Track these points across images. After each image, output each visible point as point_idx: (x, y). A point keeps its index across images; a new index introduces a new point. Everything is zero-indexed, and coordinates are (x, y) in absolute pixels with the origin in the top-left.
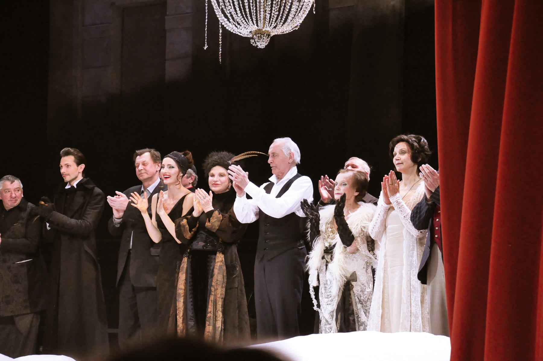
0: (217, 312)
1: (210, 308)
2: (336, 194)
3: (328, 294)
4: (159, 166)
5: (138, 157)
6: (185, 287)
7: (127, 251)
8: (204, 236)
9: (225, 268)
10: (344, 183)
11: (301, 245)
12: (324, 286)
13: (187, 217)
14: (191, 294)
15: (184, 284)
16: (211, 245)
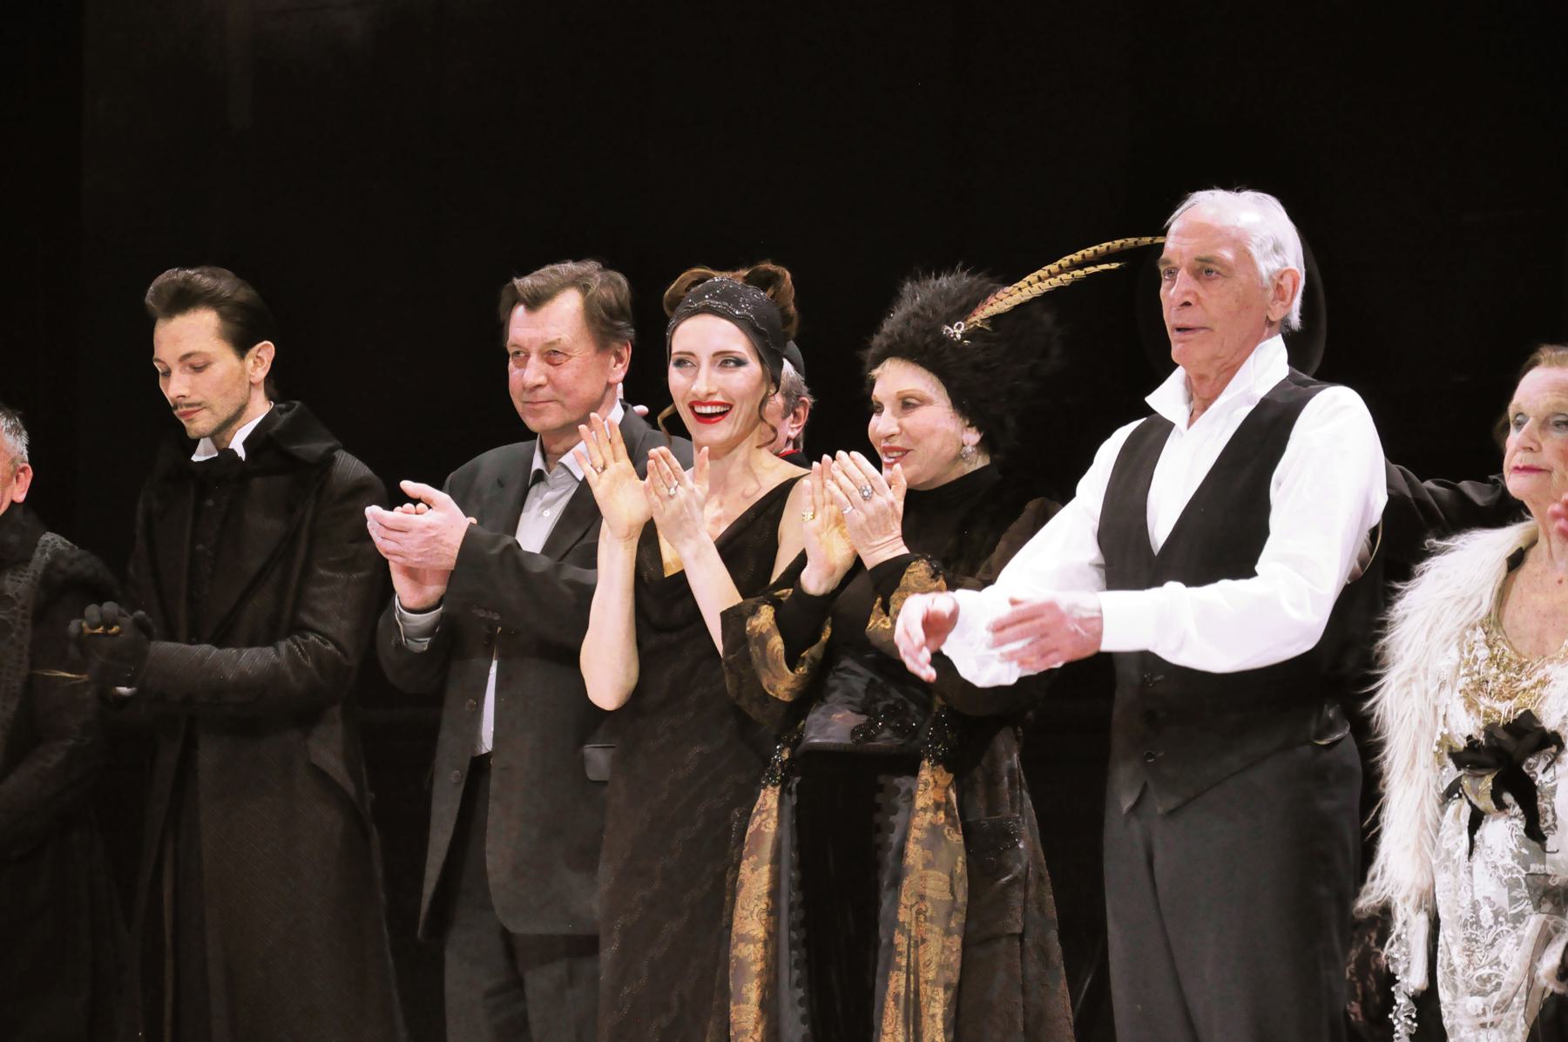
2: (1517, 468)
3: (1485, 972)
6: (768, 932)
8: (859, 685)
9: (956, 838)
11: (1331, 727)
12: (1461, 934)
13: (777, 593)
14: (797, 965)
15: (764, 916)
16: (894, 729)
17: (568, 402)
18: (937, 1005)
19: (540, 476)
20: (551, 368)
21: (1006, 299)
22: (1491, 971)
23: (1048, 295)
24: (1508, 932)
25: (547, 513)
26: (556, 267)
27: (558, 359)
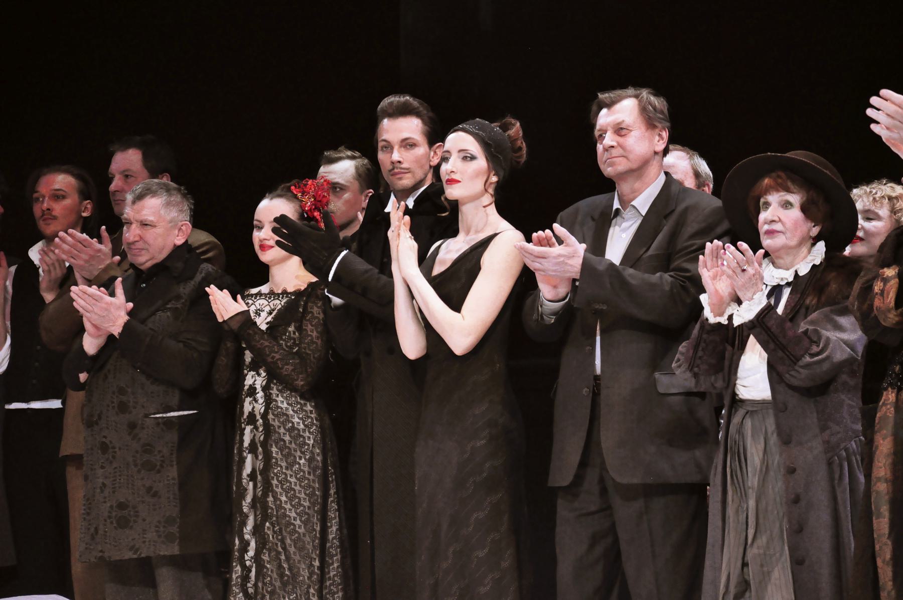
4: (663, 139)
5: (604, 111)
7: (592, 383)
20: (620, 137)
25: (624, 235)
27: (624, 132)
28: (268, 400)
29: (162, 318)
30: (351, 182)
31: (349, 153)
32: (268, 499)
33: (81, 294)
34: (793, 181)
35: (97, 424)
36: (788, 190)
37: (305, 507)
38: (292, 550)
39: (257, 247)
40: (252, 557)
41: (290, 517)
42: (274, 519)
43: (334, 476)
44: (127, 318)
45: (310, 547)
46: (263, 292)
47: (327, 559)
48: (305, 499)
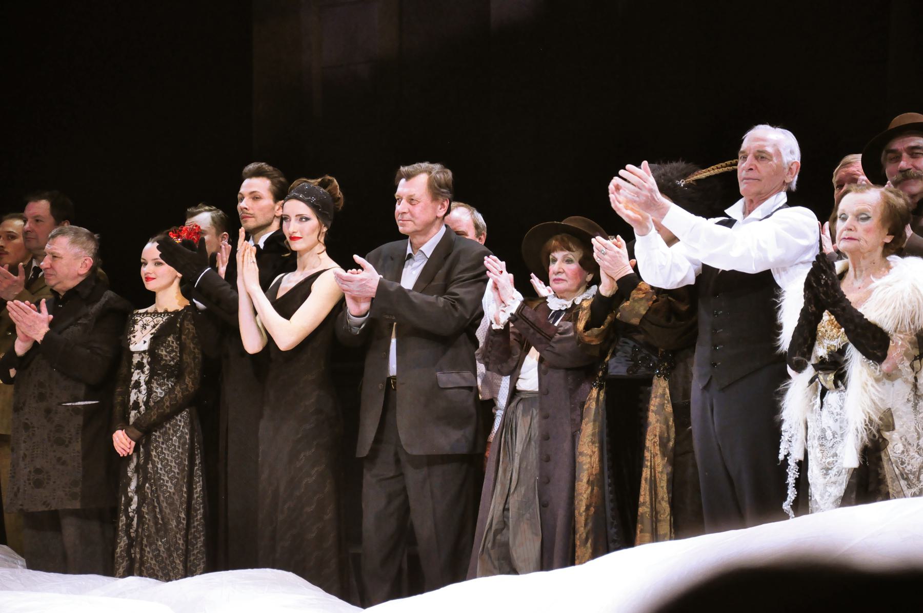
0: (660, 502)
1: (644, 496)
10: (864, 216)
17: (417, 221)
18: (664, 482)
19: (410, 256)
20: (411, 206)
21: (703, 174)
22: (833, 459)
23: (716, 176)
24: (840, 441)
25: (414, 272)
26: (421, 164)
28: (150, 392)
29: (74, 331)
30: (209, 228)
31: (207, 208)
32: (148, 466)
33: (14, 307)
34: (574, 243)
35: (22, 410)
36: (569, 249)
37: (174, 472)
38: (164, 505)
39: (144, 280)
40: (134, 510)
41: (163, 480)
42: (152, 481)
43: (199, 451)
44: (48, 329)
45: (178, 504)
46: (149, 312)
47: (193, 513)
48: (175, 467)
